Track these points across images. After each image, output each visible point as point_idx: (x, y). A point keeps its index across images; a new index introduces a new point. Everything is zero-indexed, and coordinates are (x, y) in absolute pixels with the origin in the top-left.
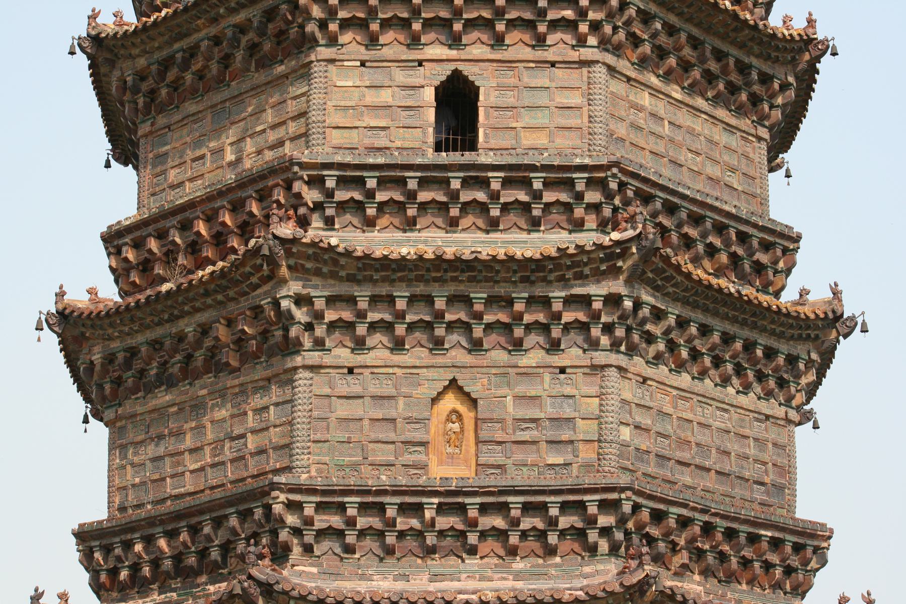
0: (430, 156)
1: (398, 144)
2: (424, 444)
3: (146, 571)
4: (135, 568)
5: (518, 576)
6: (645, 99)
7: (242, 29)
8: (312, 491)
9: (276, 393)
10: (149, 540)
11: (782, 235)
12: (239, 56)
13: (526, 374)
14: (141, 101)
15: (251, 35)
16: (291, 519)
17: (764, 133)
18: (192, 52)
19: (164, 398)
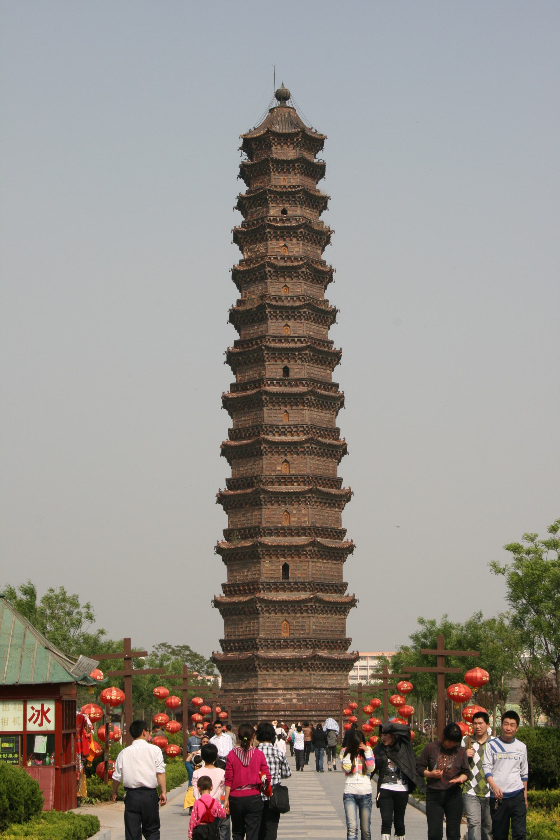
4: (231, 647)
6: (319, 564)
9: (256, 621)
10: (234, 643)
13: (298, 618)
16: (259, 643)
19: (235, 617)
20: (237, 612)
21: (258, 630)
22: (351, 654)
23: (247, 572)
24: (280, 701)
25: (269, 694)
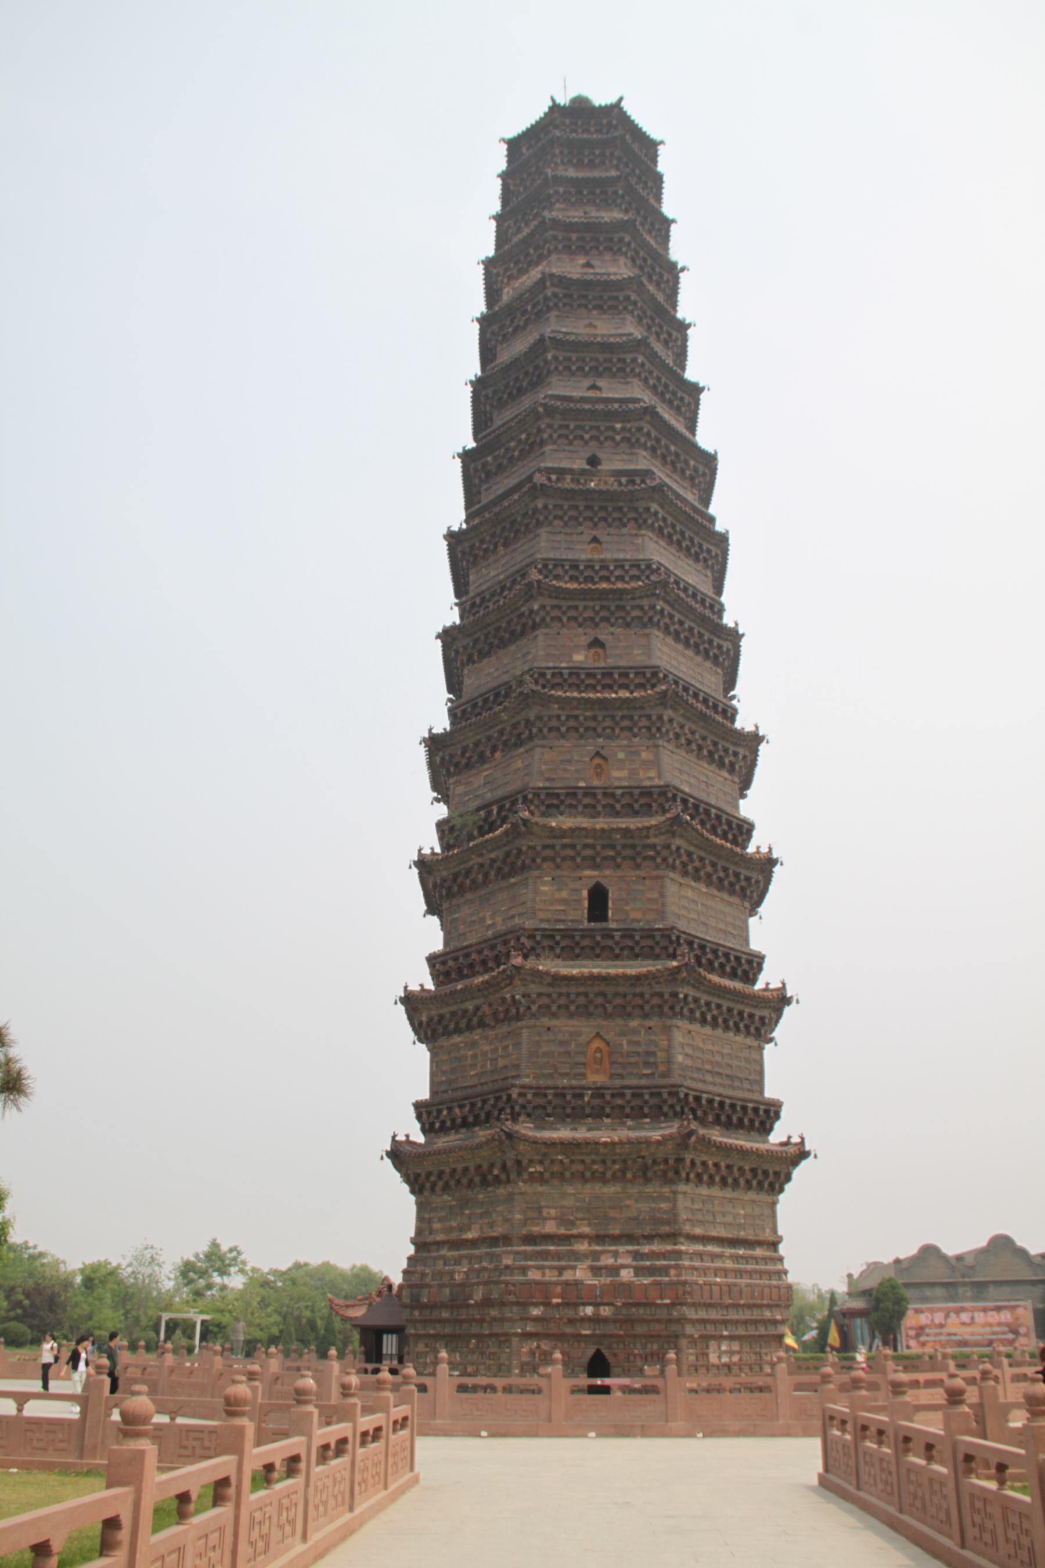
0: (586, 924)
1: (571, 918)
2: (584, 1064)
3: (448, 1124)
4: (443, 1122)
5: (630, 1129)
7: (493, 861)
8: (531, 1088)
11: (756, 956)
12: (492, 873)
13: (635, 1031)
14: (444, 892)
15: (498, 863)
17: (736, 779)
18: (468, 872)
19: (457, 1039)
20: (463, 1024)
21: (517, 1066)
22: (783, 1144)
23: (493, 916)
24: (581, 1273)
25: (548, 1252)
